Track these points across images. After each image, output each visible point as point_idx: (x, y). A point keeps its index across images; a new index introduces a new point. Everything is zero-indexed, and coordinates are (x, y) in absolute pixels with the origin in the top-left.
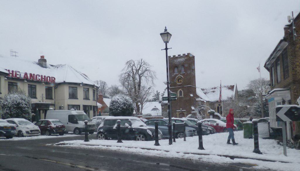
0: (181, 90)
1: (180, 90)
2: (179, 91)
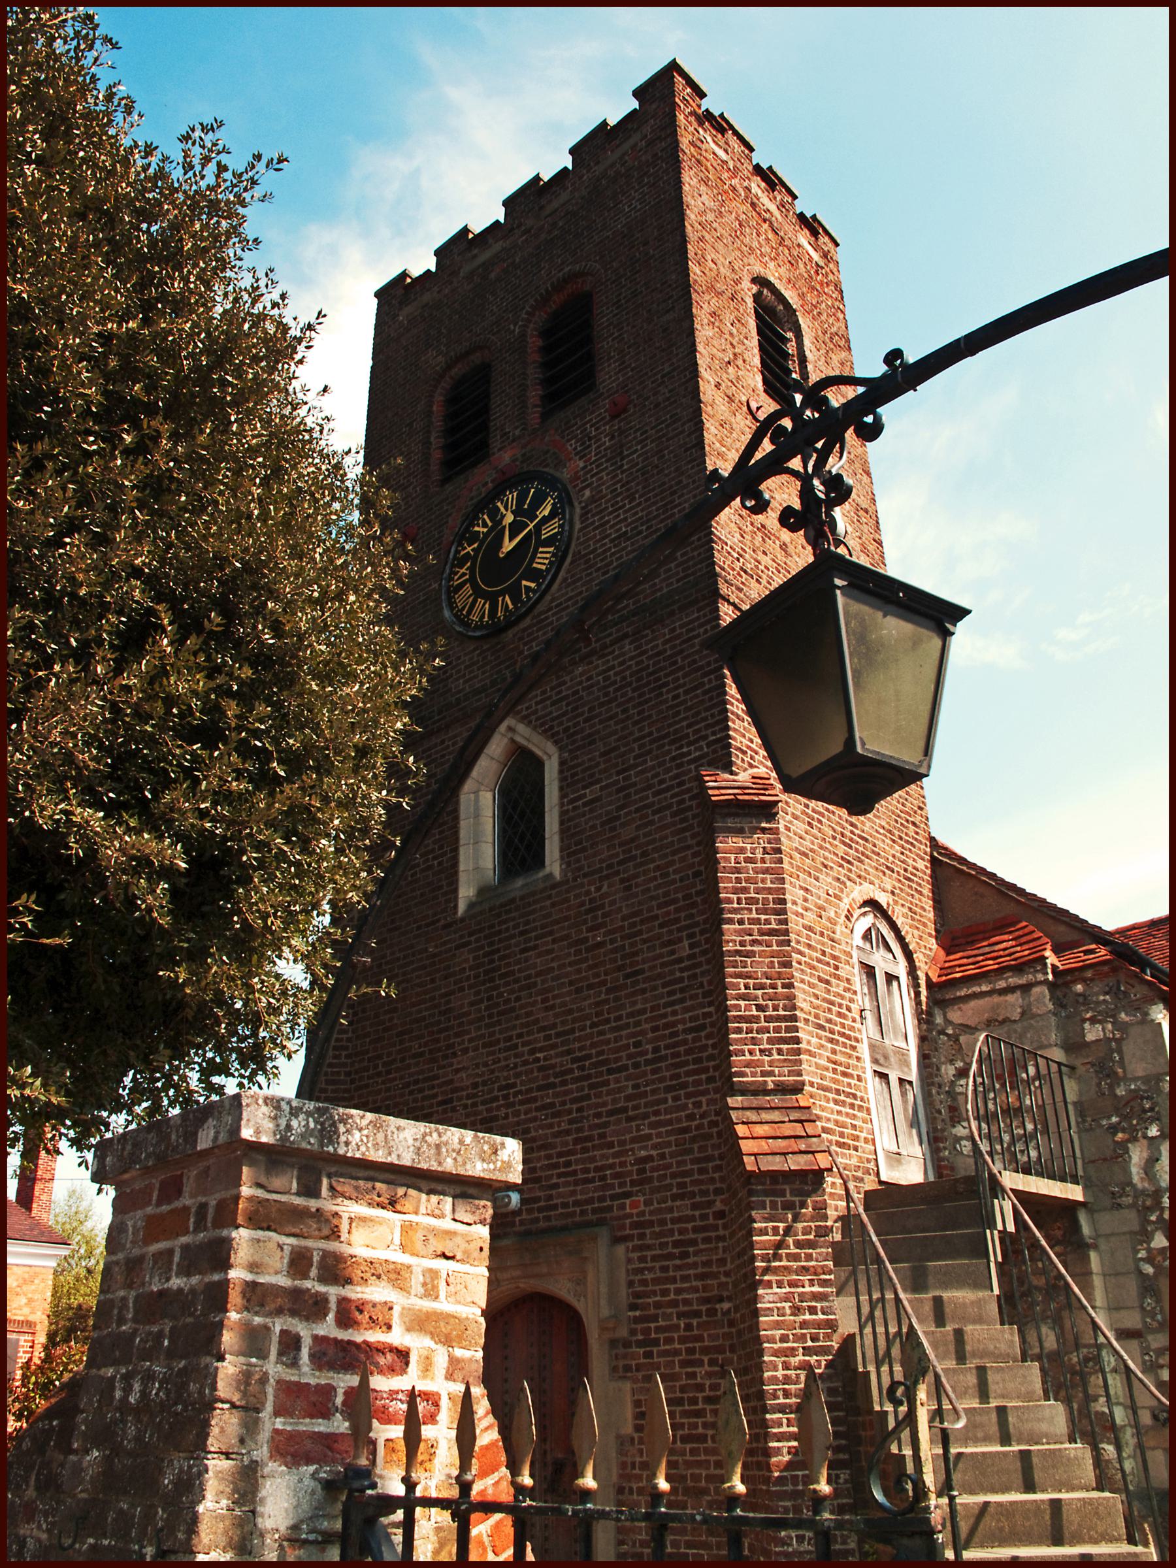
0: (525, 734)
1: (509, 722)
2: (497, 747)
